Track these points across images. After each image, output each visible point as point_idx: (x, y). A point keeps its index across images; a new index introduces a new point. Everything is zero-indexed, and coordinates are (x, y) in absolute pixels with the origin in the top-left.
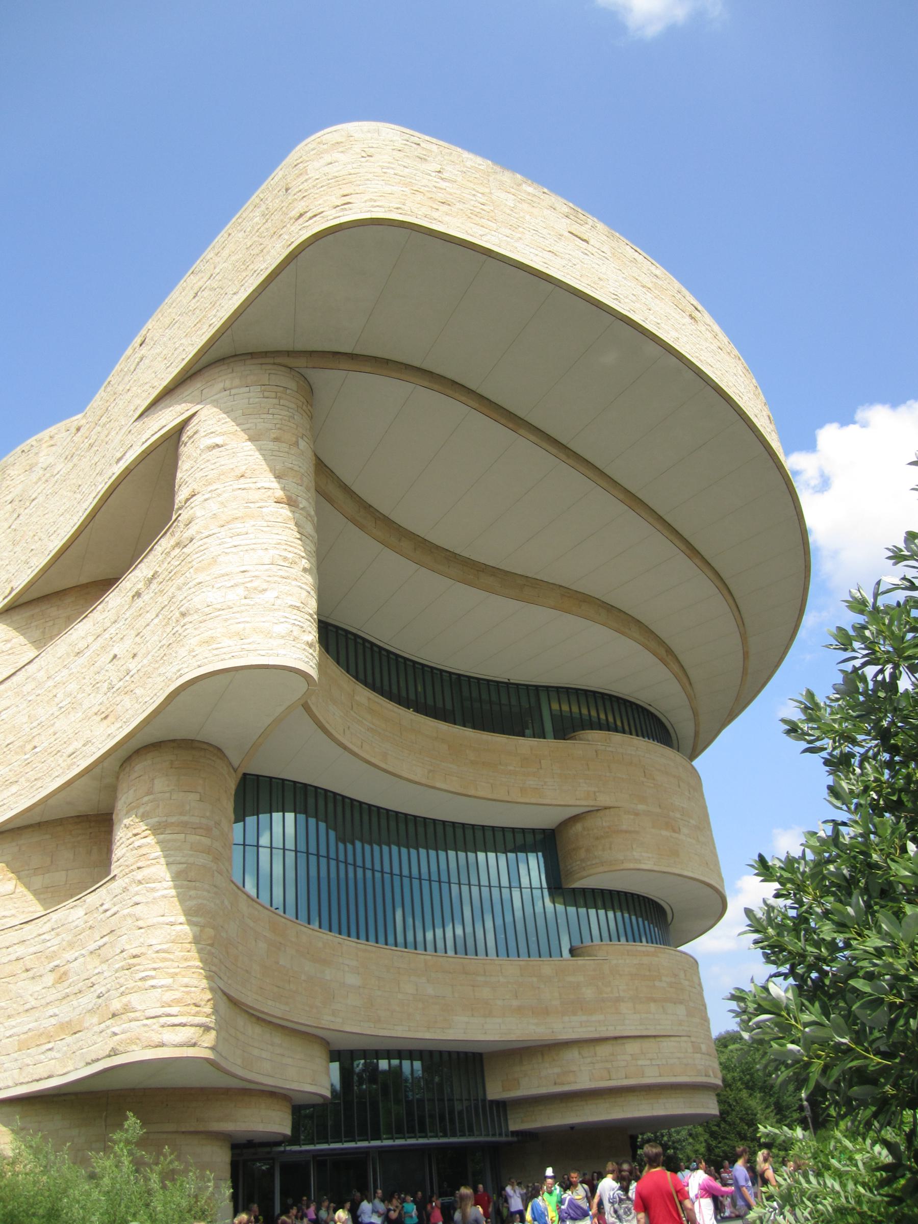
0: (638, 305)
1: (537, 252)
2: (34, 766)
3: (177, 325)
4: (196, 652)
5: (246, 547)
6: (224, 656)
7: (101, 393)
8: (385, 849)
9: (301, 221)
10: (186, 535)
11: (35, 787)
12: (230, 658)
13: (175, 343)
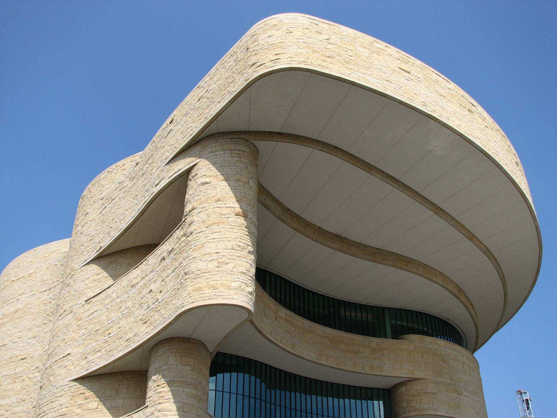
0: (437, 108)
1: (380, 82)
2: (109, 344)
3: (189, 115)
4: (192, 295)
5: (219, 240)
6: (205, 298)
7: (149, 146)
8: (293, 394)
9: (253, 67)
10: (189, 230)
11: (109, 355)
12: (208, 299)
13: (187, 125)
